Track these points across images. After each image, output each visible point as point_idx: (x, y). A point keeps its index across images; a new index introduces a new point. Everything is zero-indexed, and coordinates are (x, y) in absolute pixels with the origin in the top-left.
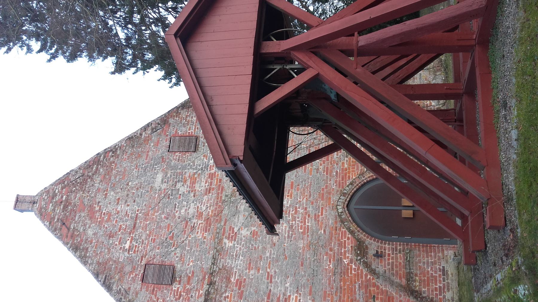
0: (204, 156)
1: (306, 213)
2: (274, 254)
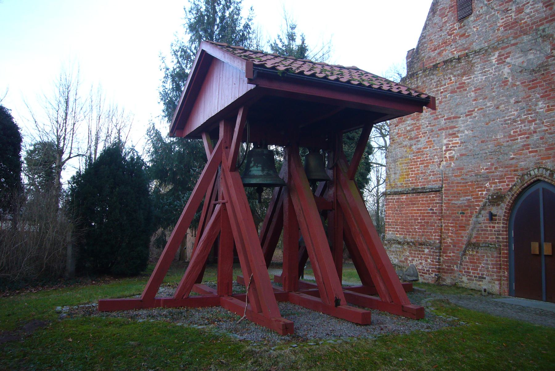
1: (530, 134)
2: (489, 110)
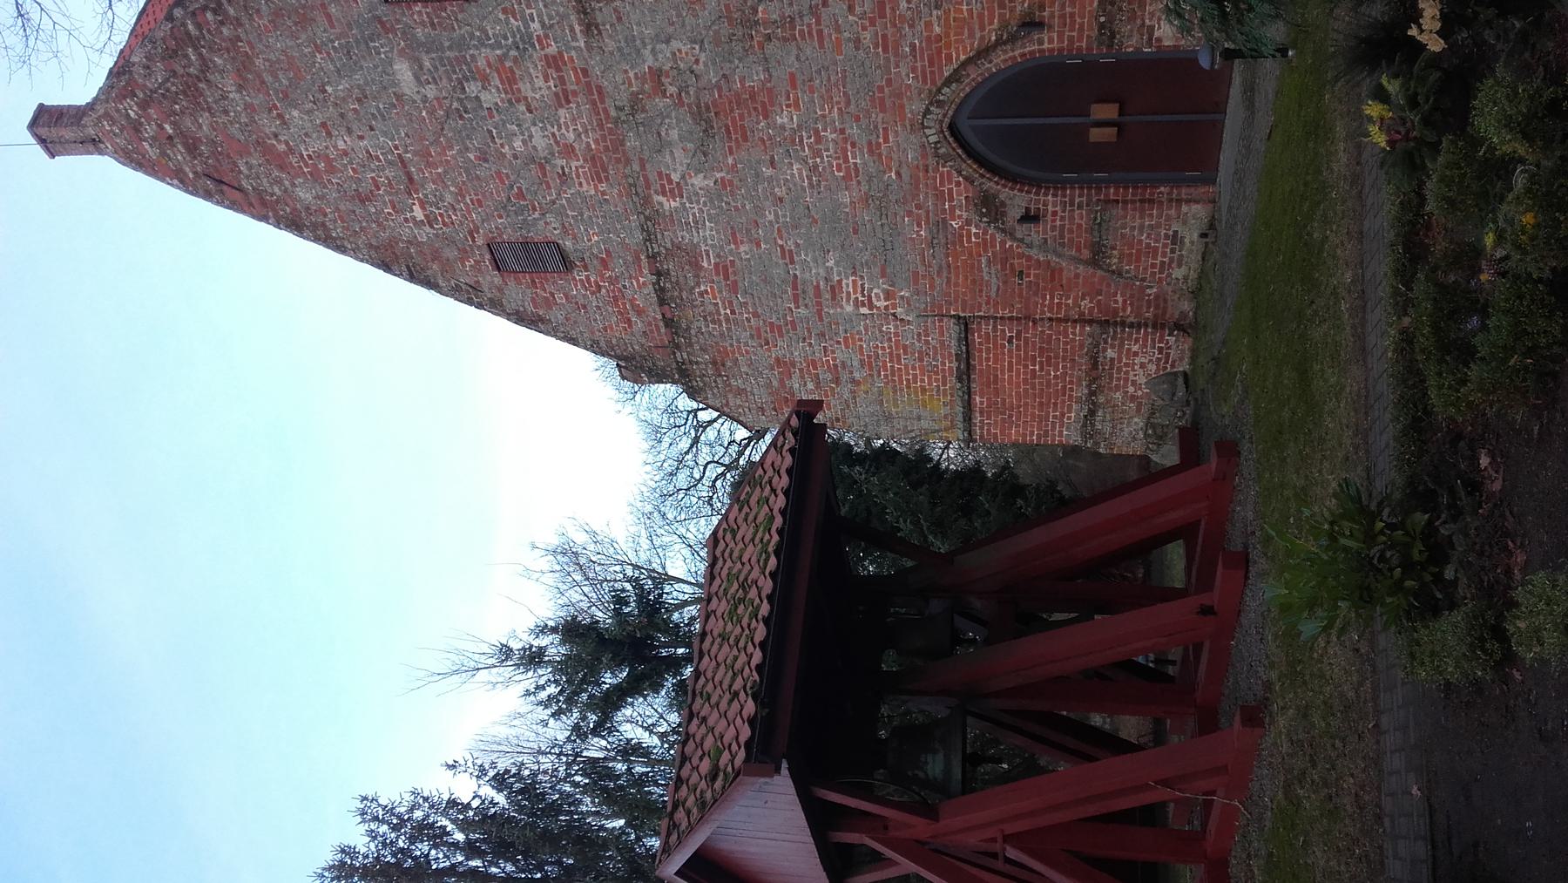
0: (505, 11)
1: (845, 140)
2: (785, 216)
